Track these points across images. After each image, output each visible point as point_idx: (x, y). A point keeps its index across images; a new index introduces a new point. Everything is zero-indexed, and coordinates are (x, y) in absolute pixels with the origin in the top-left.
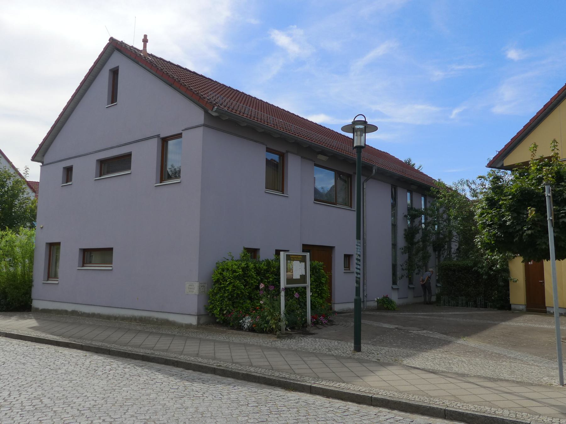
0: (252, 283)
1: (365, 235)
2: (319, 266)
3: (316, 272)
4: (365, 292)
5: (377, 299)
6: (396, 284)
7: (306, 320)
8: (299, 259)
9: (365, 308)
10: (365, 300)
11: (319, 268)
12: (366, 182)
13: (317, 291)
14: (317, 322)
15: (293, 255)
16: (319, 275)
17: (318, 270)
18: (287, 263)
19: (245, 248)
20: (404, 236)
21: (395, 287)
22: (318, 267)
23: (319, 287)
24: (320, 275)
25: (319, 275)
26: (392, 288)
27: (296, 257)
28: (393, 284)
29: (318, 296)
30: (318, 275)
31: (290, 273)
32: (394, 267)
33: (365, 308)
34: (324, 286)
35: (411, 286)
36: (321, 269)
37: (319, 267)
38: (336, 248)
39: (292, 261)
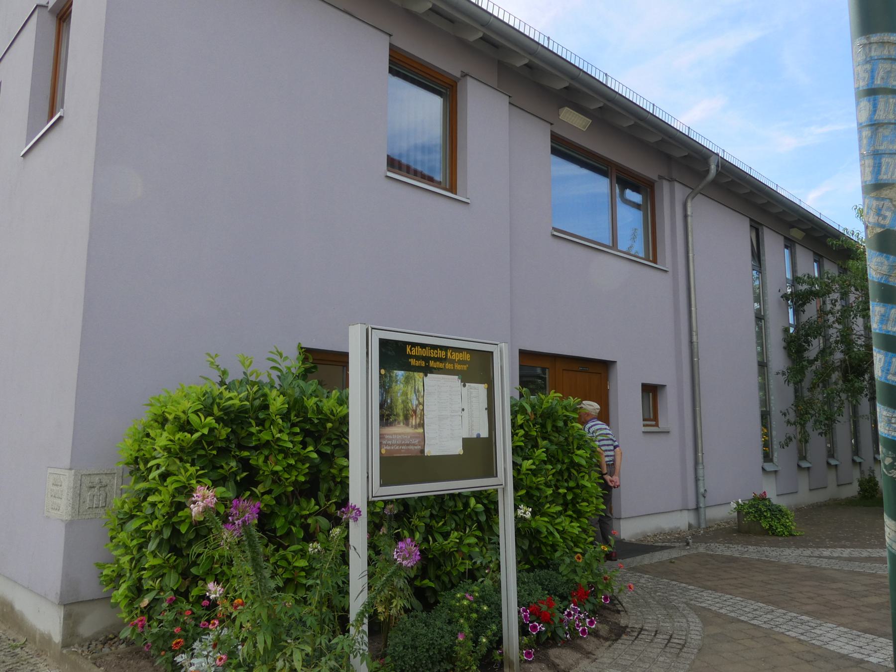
0: (275, 473)
1: (694, 333)
2: (565, 408)
3: (557, 429)
4: (701, 484)
5: (738, 503)
6: (771, 461)
7: (498, 642)
8: (458, 367)
9: (703, 526)
10: (701, 505)
11: (565, 416)
12: (693, 198)
13: (559, 494)
14: (554, 633)
15: (423, 346)
16: (566, 439)
17: (560, 424)
18: (385, 386)
19: (302, 348)
20: (784, 344)
21: (769, 467)
22: (561, 411)
23: (566, 481)
24: (571, 439)
25: (566, 439)
26: (763, 469)
27: (442, 354)
28: (765, 462)
29: (565, 510)
30: (562, 439)
31: (409, 430)
32: (765, 417)
33: (703, 526)
34: (583, 477)
35: (804, 464)
36: (574, 418)
37: (568, 414)
38: (619, 365)
39: (418, 376)
